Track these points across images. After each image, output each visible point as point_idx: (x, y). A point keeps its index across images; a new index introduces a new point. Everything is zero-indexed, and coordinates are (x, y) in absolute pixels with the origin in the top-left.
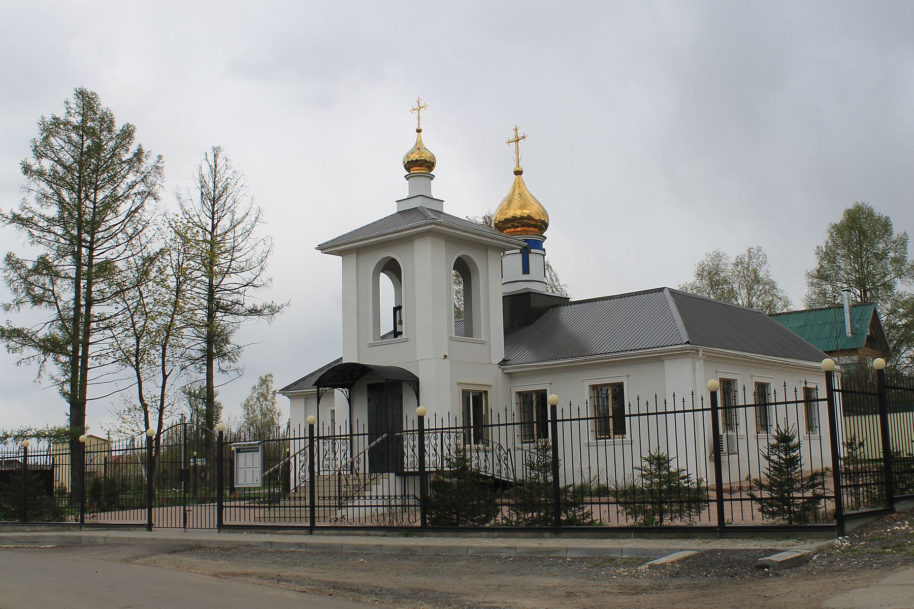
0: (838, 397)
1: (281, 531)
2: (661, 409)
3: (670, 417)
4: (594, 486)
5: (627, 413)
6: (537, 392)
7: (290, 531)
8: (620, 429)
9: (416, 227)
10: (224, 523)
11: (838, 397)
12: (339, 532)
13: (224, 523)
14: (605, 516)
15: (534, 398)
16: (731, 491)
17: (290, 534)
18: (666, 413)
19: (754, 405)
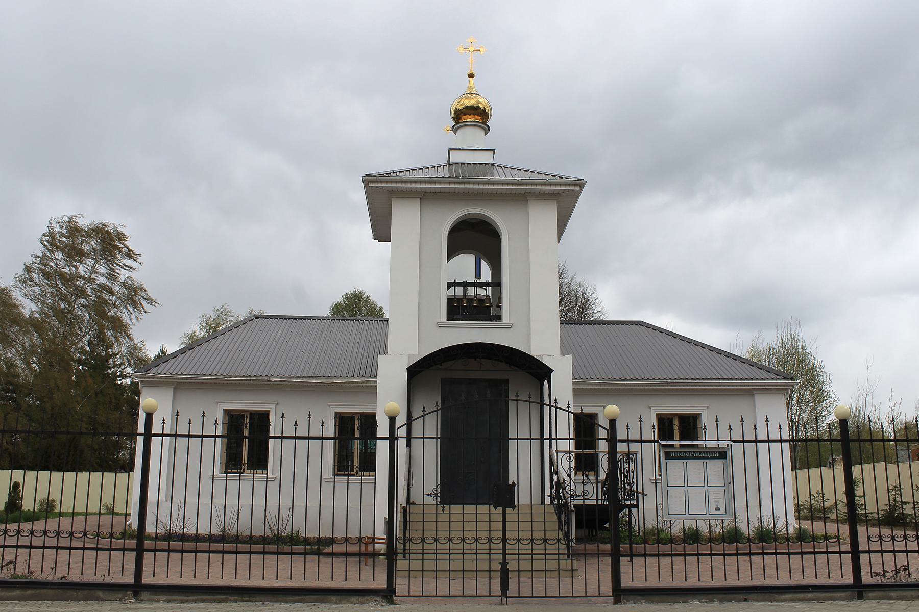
0: (141, 428)
1: (788, 596)
2: (749, 436)
3: (763, 446)
4: (677, 530)
5: (439, 440)
6: (253, 414)
7: (810, 595)
8: (259, 461)
9: (464, 183)
10: (623, 585)
11: (141, 428)
12: (880, 593)
13: (623, 585)
14: (35, 566)
15: (247, 421)
16: (157, 538)
17: (810, 600)
18: (769, 441)
19: (398, 437)
